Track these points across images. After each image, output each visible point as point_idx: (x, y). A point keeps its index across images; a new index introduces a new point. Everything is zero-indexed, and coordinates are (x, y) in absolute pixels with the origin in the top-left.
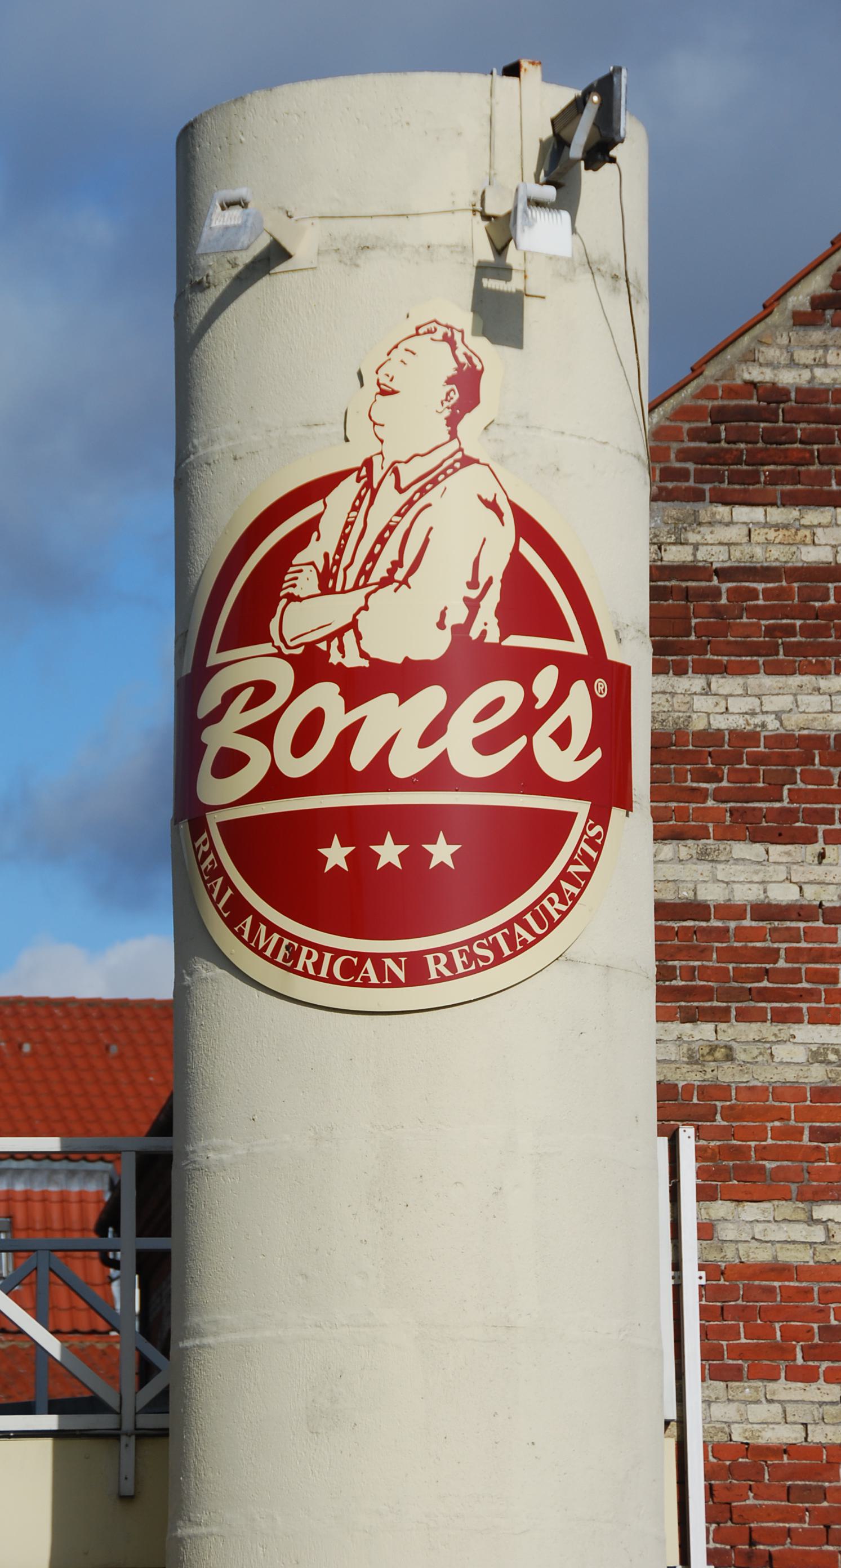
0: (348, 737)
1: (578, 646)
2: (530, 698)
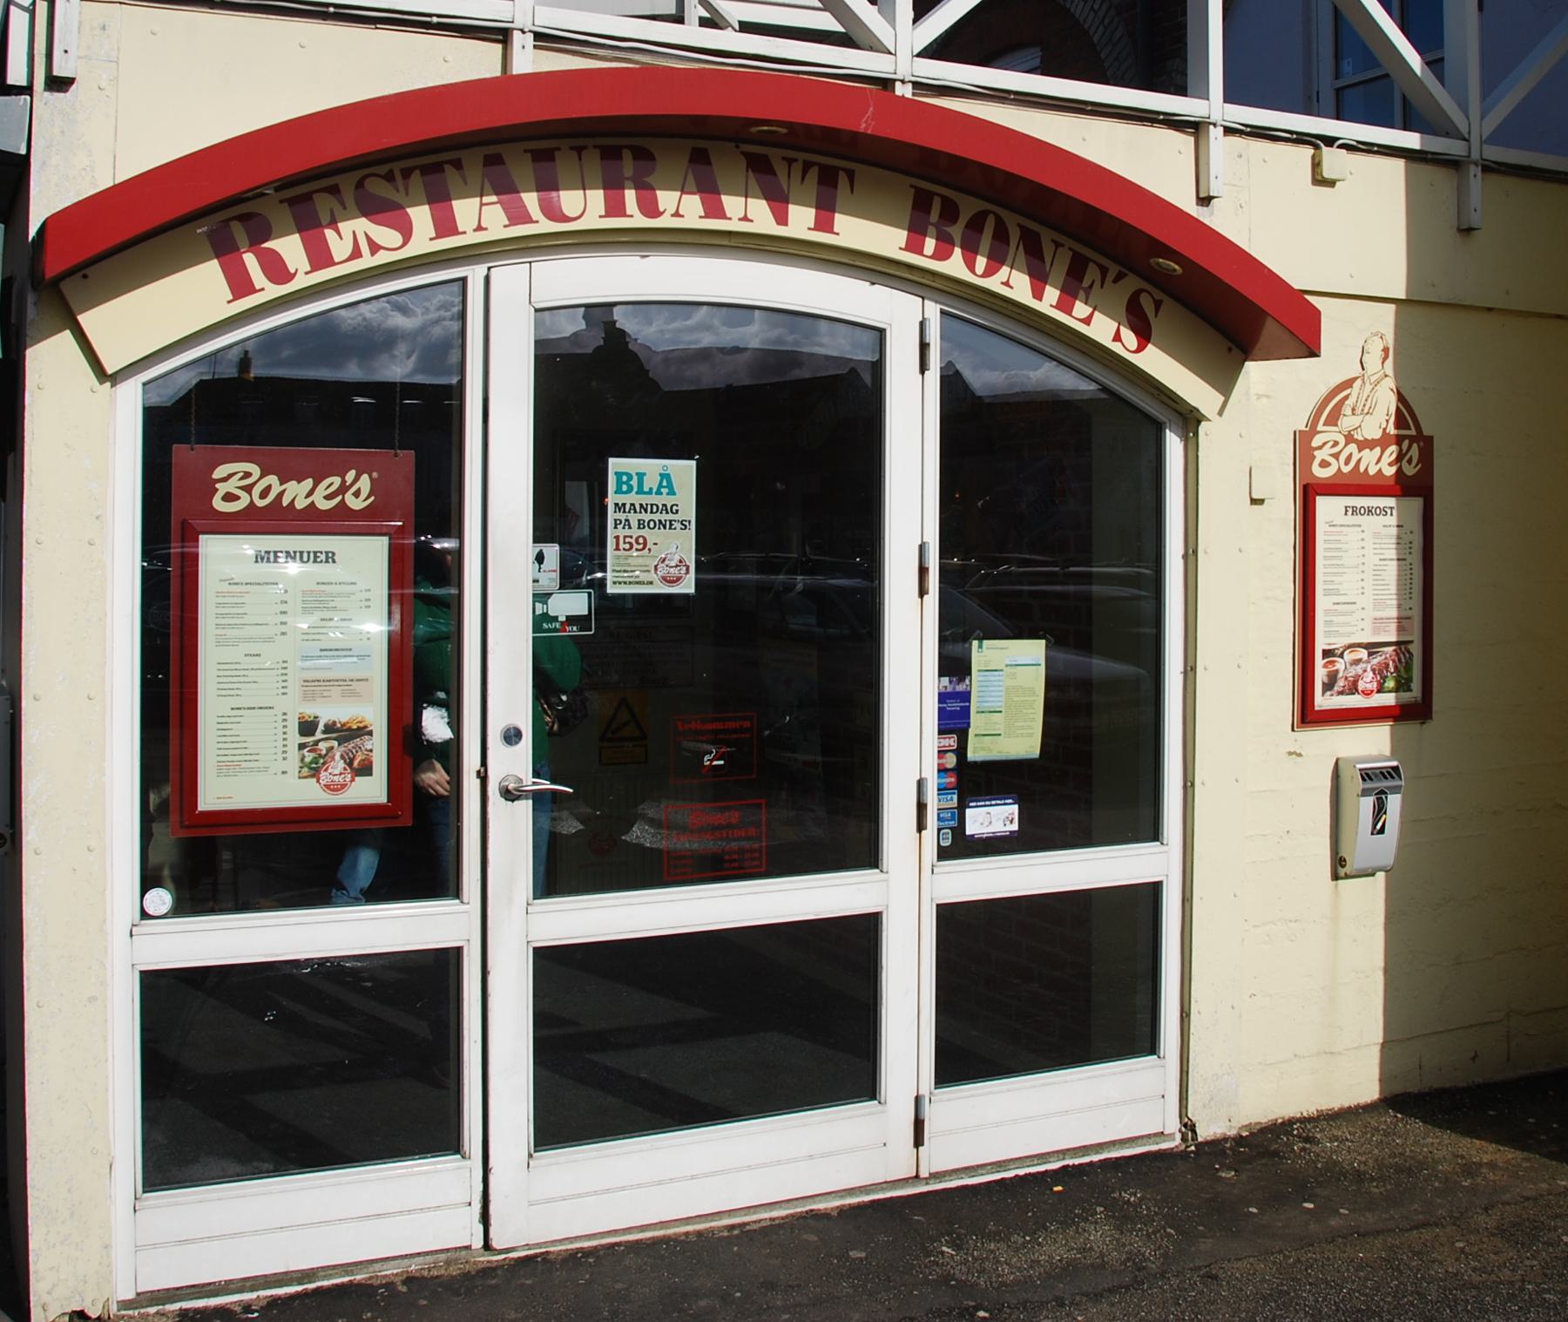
0: (281, 494)
1: (1413, 432)
2: (344, 481)
